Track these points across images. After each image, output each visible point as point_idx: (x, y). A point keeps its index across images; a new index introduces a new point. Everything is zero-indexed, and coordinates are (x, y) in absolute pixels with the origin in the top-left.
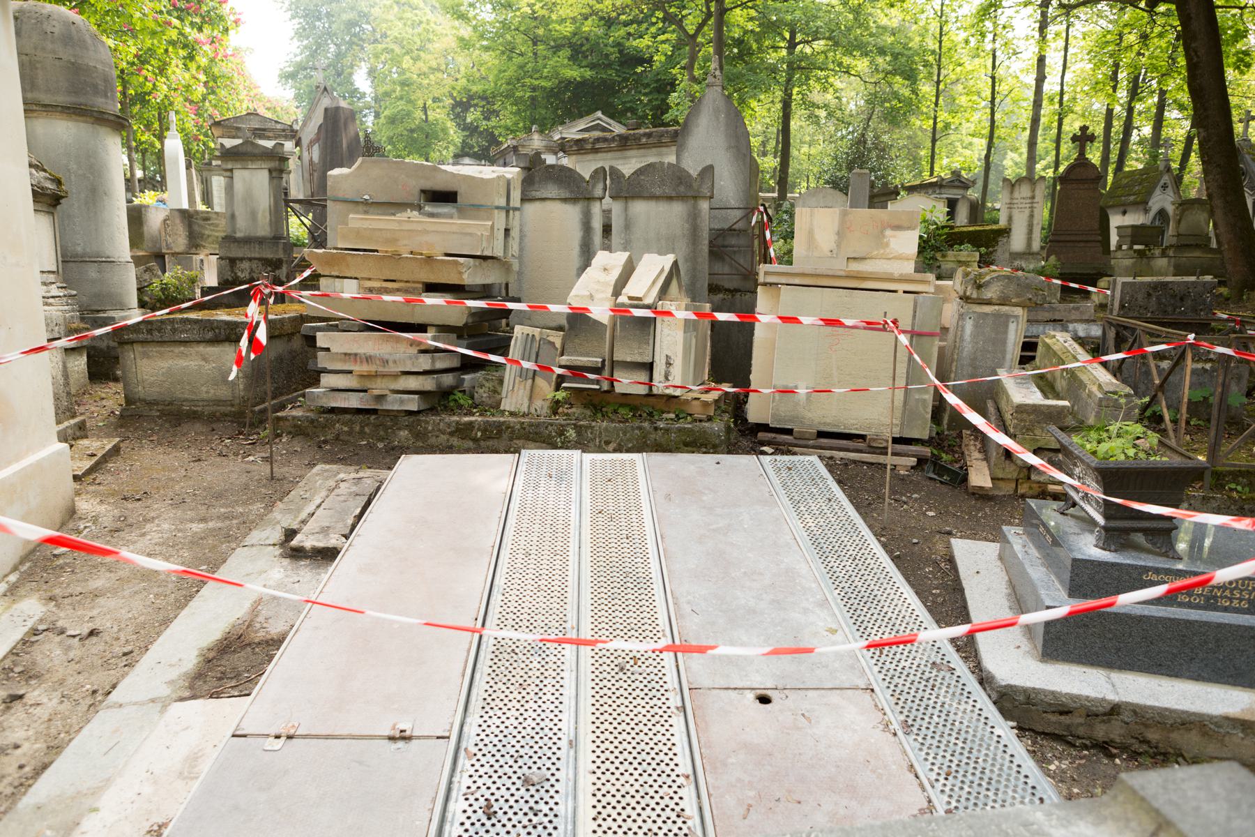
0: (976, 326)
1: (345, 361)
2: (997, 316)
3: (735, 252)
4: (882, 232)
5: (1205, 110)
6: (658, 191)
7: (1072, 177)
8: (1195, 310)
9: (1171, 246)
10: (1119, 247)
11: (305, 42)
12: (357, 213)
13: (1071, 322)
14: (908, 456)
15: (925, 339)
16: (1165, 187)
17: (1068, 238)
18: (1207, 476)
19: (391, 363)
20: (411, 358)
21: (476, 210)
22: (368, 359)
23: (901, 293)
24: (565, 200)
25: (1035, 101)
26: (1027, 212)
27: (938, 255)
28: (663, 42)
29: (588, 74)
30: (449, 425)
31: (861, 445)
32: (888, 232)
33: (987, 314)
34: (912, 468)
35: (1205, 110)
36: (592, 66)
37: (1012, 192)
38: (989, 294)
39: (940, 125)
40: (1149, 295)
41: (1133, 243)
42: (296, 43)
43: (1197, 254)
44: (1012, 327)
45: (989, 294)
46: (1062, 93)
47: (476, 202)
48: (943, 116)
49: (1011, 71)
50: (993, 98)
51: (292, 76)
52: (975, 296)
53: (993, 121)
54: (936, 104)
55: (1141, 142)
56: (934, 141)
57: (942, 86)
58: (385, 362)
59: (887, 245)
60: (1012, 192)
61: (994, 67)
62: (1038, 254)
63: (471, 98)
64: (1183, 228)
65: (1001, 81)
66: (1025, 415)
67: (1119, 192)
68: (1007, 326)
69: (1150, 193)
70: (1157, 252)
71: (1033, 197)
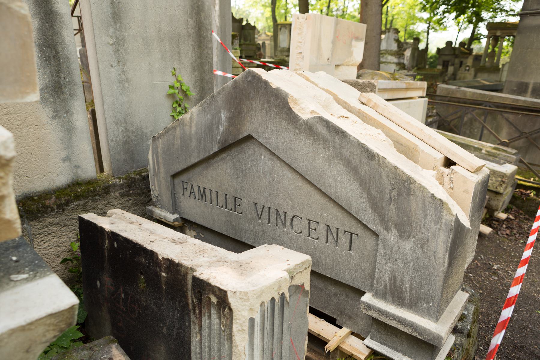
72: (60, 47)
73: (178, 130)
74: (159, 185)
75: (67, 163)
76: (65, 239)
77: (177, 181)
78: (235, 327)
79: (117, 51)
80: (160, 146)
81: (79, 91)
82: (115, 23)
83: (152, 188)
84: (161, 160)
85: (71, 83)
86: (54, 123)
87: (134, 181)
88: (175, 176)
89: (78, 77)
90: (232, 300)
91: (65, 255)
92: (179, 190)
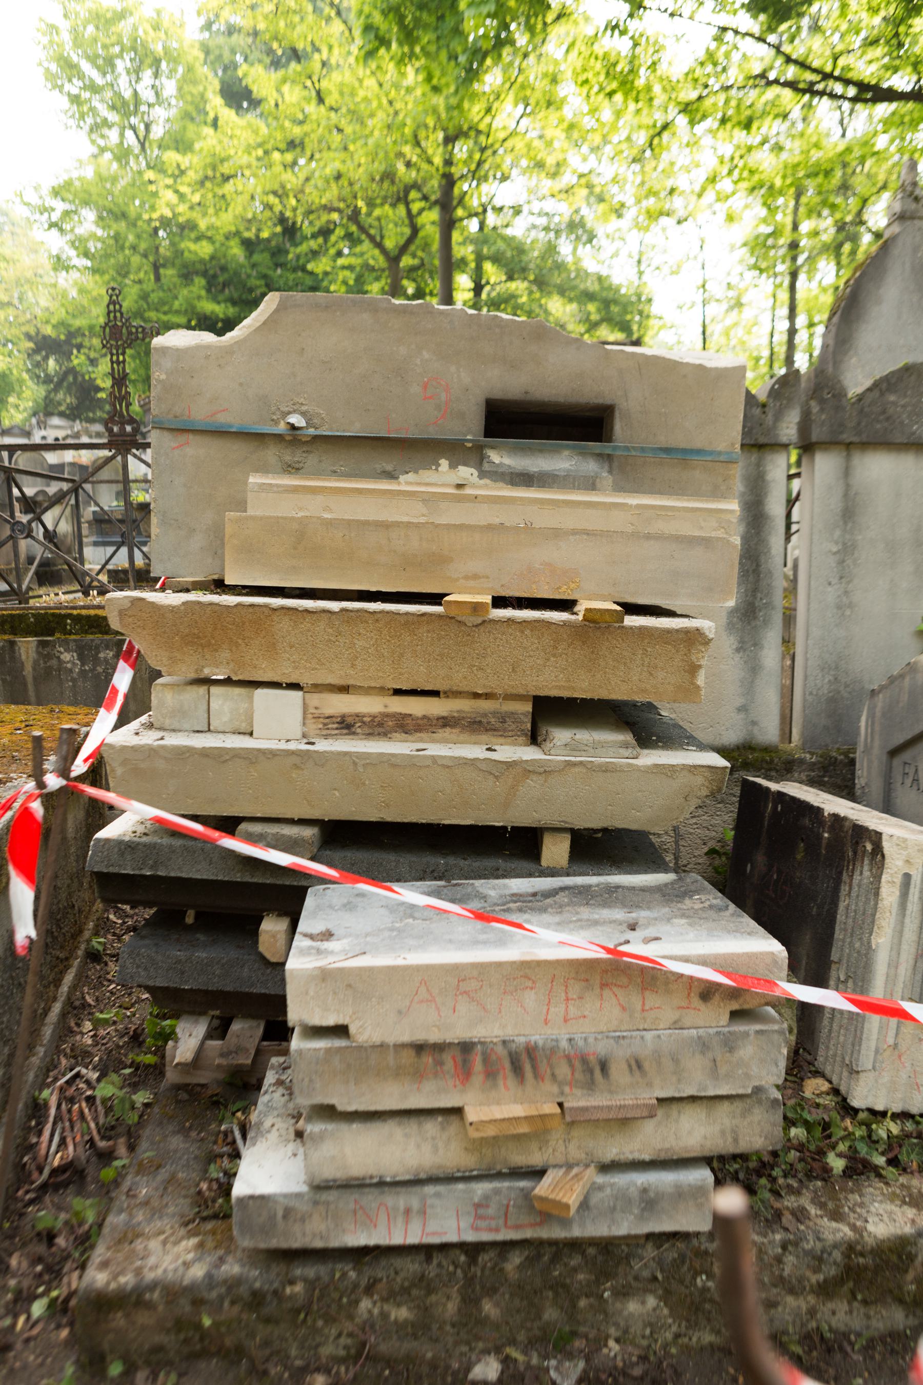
1: (418, 1075)
12: (264, 469)
19: (618, 1071)
20: (703, 1045)
21: (675, 462)
22: (522, 1062)
28: (343, 268)
30: (818, 1260)
47: (679, 440)
58: (593, 1069)
63: (71, 335)
72: (763, 559)
73: (907, 681)
74: (869, 768)
75: (742, 716)
76: (717, 821)
77: (897, 762)
78: (884, 878)
79: (841, 562)
80: (880, 705)
81: (777, 619)
82: (845, 523)
83: (858, 773)
84: (877, 728)
85: (769, 605)
86: (737, 657)
87: (834, 762)
88: (894, 753)
89: (779, 601)
90: (886, 845)
91: (712, 844)
92: (897, 777)
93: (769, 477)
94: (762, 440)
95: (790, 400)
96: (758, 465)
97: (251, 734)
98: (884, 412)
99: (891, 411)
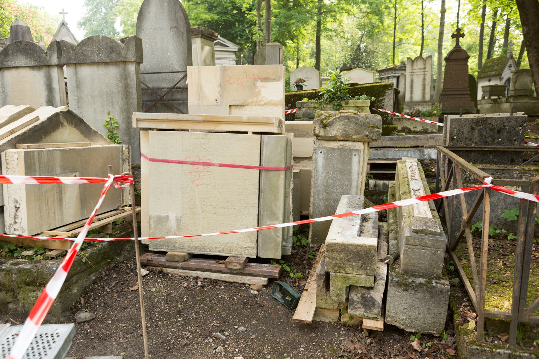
0: (326, 159)
2: (342, 150)
3: (180, 104)
4: (254, 84)
5: (527, 15)
6: (96, 59)
7: (453, 57)
8: (510, 141)
9: (511, 96)
10: (483, 98)
11: (90, 7)
13: (426, 148)
14: (260, 276)
15: (272, 173)
16: (510, 66)
17: (451, 93)
18: (513, 328)
23: (250, 134)
24: (32, 67)
25: (441, 23)
26: (422, 77)
27: (343, 103)
29: (216, 17)
31: (221, 266)
32: (259, 84)
33: (334, 149)
34: (264, 286)
35: (527, 15)
36: (218, 14)
37: (412, 66)
38: (334, 132)
39: (397, 40)
40: (473, 129)
41: (491, 95)
42: (85, 8)
43: (526, 100)
44: (355, 159)
45: (334, 132)
46: (458, 22)
48: (398, 35)
49: (431, 11)
50: (423, 25)
51: (84, 24)
52: (322, 134)
53: (423, 37)
54: (395, 29)
55: (499, 47)
56: (394, 48)
57: (397, 20)
58: (479, 273)
59: (259, 93)
60: (412, 66)
61: (423, 9)
62: (429, 102)
64: (518, 86)
65: (426, 16)
66: (335, 254)
67: (487, 70)
68: (351, 159)
69: (502, 70)
70: (504, 100)
71: (425, 68)
72: (54, 102)
93: (53, 76)
94: (47, 64)
95: (53, 51)
96: (49, 72)
97: (230, 106)
98: (83, 53)
99: (85, 52)
